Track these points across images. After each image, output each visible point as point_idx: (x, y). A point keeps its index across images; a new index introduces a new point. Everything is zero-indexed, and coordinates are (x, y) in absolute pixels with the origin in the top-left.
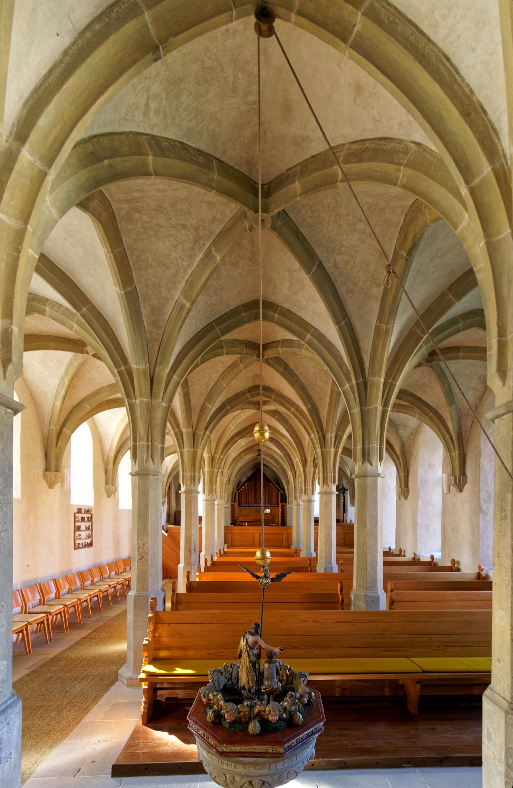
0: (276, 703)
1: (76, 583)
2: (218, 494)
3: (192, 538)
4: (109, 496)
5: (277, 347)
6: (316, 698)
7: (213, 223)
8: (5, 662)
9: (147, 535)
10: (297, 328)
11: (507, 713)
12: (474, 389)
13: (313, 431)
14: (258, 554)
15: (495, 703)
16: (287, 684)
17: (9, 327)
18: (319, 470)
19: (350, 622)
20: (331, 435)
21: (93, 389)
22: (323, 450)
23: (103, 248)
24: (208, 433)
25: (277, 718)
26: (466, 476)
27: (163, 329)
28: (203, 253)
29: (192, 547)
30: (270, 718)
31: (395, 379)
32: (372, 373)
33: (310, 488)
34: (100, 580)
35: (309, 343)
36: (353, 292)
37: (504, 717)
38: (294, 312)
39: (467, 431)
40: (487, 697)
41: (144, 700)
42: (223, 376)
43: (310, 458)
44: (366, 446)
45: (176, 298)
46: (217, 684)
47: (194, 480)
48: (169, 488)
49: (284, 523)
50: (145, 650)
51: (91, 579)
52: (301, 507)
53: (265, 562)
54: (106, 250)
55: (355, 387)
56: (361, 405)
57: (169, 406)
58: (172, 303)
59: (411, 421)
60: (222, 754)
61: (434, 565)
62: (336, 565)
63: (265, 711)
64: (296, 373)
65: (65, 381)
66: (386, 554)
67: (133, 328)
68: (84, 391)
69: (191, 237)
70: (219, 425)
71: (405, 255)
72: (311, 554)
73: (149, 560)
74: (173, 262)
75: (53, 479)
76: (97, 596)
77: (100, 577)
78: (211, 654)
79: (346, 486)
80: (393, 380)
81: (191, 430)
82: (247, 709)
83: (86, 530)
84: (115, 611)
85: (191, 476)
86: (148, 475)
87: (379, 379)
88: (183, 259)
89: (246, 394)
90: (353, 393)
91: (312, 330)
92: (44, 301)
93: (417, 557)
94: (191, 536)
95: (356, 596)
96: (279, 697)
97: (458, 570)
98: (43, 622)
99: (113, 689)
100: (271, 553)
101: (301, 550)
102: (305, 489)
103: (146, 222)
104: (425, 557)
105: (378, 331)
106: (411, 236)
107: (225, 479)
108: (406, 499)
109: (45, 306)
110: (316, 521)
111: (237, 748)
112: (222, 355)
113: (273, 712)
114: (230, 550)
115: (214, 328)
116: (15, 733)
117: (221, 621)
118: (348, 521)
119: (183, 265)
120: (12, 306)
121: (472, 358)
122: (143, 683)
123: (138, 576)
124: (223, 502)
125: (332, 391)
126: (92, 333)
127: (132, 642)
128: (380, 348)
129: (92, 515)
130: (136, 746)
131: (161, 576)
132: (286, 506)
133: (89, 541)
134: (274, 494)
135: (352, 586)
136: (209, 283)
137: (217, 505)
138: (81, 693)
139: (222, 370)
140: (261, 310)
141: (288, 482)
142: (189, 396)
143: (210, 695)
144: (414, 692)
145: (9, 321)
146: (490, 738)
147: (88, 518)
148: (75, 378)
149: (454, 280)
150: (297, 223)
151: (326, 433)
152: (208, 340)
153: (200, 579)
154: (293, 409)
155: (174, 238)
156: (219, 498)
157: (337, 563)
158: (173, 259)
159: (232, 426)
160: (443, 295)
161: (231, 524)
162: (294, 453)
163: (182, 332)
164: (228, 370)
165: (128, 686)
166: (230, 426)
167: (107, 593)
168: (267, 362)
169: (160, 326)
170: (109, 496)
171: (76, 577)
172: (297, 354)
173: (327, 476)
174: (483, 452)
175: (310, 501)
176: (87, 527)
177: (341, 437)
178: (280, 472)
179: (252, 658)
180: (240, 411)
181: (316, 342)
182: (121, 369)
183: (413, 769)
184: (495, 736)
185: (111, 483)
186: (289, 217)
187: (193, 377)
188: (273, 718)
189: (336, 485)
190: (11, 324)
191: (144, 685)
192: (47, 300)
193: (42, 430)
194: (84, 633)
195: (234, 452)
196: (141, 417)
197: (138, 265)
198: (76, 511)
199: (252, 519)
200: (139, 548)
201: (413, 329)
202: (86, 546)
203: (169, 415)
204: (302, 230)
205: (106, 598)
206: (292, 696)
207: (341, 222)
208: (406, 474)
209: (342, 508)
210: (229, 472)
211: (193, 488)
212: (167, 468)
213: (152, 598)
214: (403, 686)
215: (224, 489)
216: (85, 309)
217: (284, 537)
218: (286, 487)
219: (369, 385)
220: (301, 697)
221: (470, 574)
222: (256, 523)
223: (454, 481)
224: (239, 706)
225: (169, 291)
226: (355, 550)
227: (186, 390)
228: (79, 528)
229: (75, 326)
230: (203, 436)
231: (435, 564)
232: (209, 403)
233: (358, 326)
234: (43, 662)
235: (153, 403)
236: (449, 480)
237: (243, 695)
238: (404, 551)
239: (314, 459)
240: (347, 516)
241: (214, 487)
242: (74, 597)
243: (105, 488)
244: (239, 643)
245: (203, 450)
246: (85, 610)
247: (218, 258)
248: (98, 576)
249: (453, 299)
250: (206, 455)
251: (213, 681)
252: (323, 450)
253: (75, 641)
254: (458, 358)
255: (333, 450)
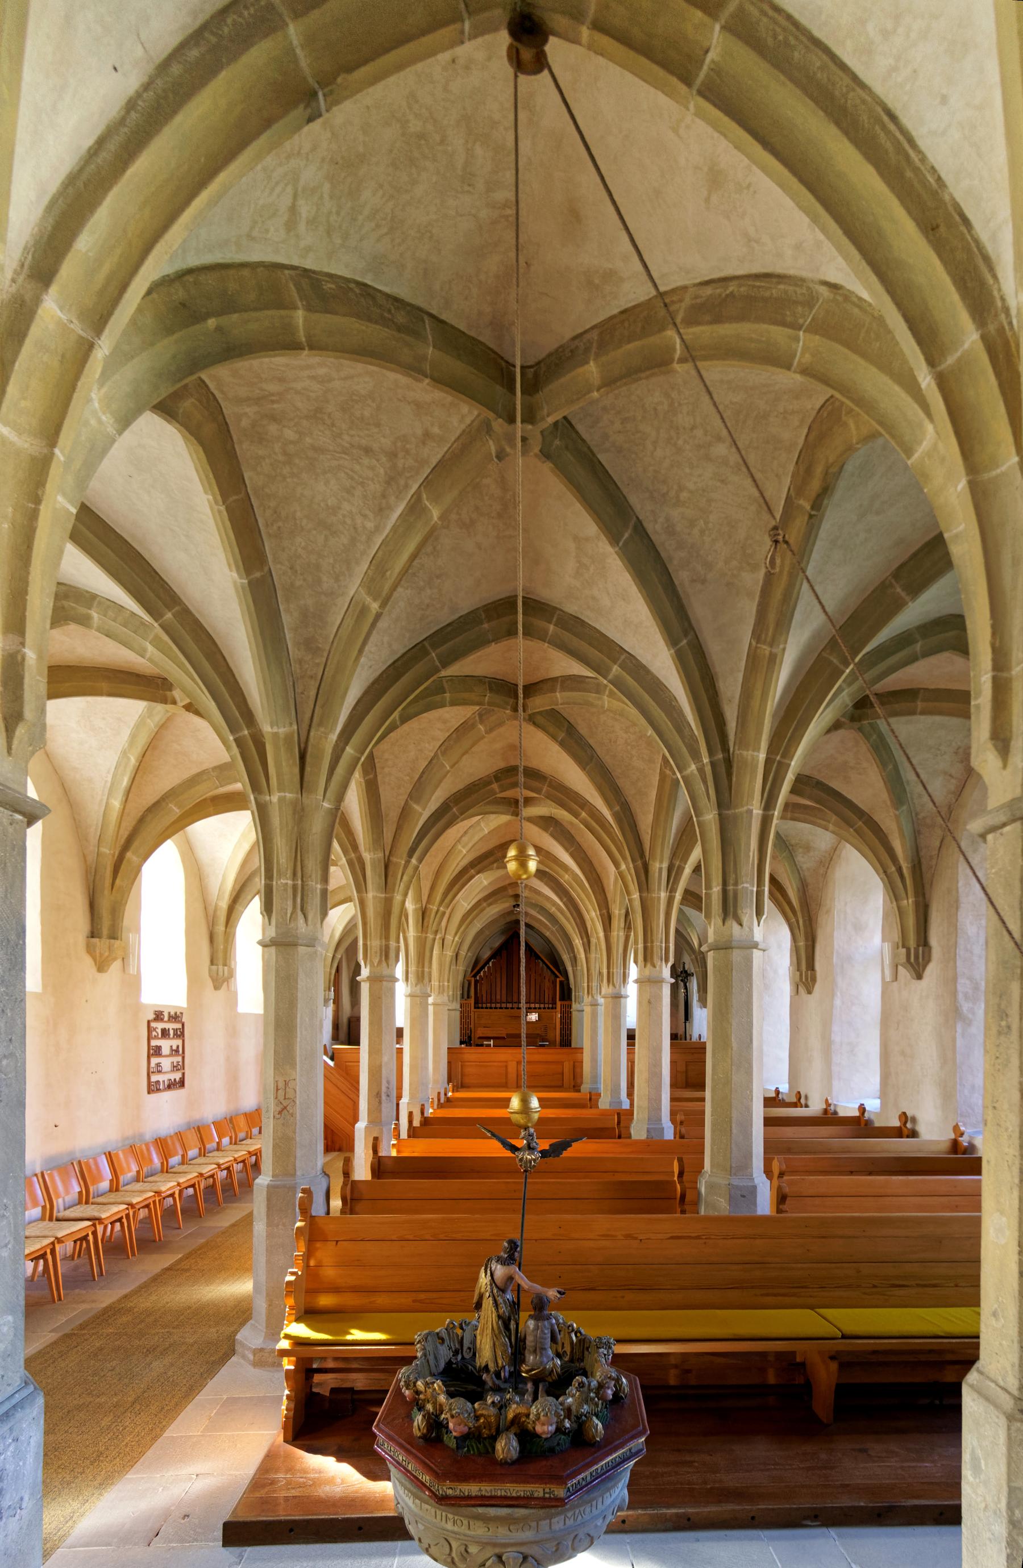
0: (551, 1399)
1: (151, 1160)
2: (435, 983)
3: (384, 1071)
4: (217, 988)
5: (553, 690)
6: (631, 1388)
7: (424, 443)
8: (10, 1318)
9: (293, 1065)
10: (593, 653)
11: (1010, 1418)
12: (945, 773)
13: (624, 858)
14: (515, 1103)
15: (987, 1399)
16: (572, 1360)
17: (18, 652)
18: (636, 936)
19: (698, 1237)
20: (659, 866)
21: (186, 775)
22: (645, 895)
23: (206, 493)
24: (414, 861)
25: (552, 1428)
26: (930, 948)
27: (325, 654)
28: (405, 502)
29: (384, 1089)
30: (539, 1429)
31: (788, 754)
32: (742, 742)
33: (617, 971)
34: (200, 1155)
35: (617, 683)
36: (704, 581)
37: (1006, 1427)
38: (586, 620)
39: (931, 857)
40: (972, 1386)
41: (287, 1392)
42: (445, 748)
43: (617, 912)
44: (730, 888)
45: (352, 593)
46: (432, 1362)
47: (387, 955)
48: (338, 970)
49: (566, 1041)
50: (289, 1293)
51: (180, 1152)
52: (601, 1010)
53: (529, 1119)
54: (211, 497)
55: (708, 769)
56: (720, 805)
57: (337, 809)
58: (343, 603)
59: (819, 837)
60: (442, 1500)
61: (866, 1125)
62: (670, 1124)
63: (528, 1416)
64: (591, 742)
65: (129, 759)
66: (770, 1102)
67: (266, 654)
68: (167, 777)
69: (382, 471)
70: (436, 845)
71: (808, 508)
72: (620, 1103)
73: (298, 1115)
74: (345, 522)
75: (107, 954)
76: (193, 1186)
77: (200, 1149)
78: (420, 1301)
79: (690, 967)
80: (783, 756)
81: (380, 855)
82: (493, 1411)
83: (171, 1055)
84: (230, 1216)
85: (381, 946)
86: (295, 945)
87: (756, 754)
88: (365, 516)
89: (490, 783)
90: (705, 782)
91: (623, 657)
92: (89, 598)
93: (832, 1107)
94: (380, 1066)
95: (711, 1186)
96: (557, 1386)
97: (914, 1134)
98: (85, 1238)
99: (224, 1371)
100: (540, 1100)
101: (600, 1095)
102: (608, 973)
103: (291, 442)
104: (848, 1108)
105: (753, 658)
106: (819, 470)
107: (449, 953)
108: (810, 992)
109: (90, 609)
110: (631, 1036)
111: (473, 1489)
112: (443, 706)
113: (543, 1416)
114: (458, 1095)
115: (427, 653)
116: (30, 1459)
117: (442, 1237)
118: (695, 1037)
119: (364, 527)
120: (25, 609)
121: (941, 713)
122: (285, 1360)
123: (276, 1146)
124: (445, 998)
125: (663, 777)
126: (183, 663)
127: (263, 1278)
128: (758, 693)
129: (183, 1025)
130: (271, 1484)
131: (321, 1147)
132: (570, 1006)
133: (177, 1076)
134: (547, 984)
135: (702, 1166)
136: (416, 563)
137: (433, 1004)
138: (162, 1380)
139: (443, 736)
140: (520, 617)
141: (574, 960)
142: (377, 788)
143: (419, 1383)
144: (826, 1377)
145: (17, 639)
146: (976, 1469)
147: (175, 1030)
148: (150, 752)
149: (905, 557)
150: (592, 444)
151: (651, 862)
152: (415, 677)
153: (398, 1152)
154: (584, 814)
155: (347, 474)
156: (437, 990)
157: (673, 1120)
158: (344, 516)
159: (463, 847)
160: (883, 587)
161: (461, 1043)
162: (587, 902)
163: (363, 660)
164: (454, 735)
165: (255, 1364)
166: (460, 847)
167: (214, 1180)
168: (532, 719)
169: (318, 648)
170: (217, 988)
171: (152, 1149)
172: (592, 705)
173: (652, 947)
174: (963, 899)
175: (618, 998)
176: (174, 1048)
177: (680, 870)
178: (558, 940)
179: (503, 1309)
180: (479, 817)
181: (630, 681)
182: (241, 734)
183: (824, 1530)
184: (986, 1464)
185: (221, 961)
186: (577, 432)
187: (385, 751)
188: (545, 1429)
189: (670, 964)
190: (23, 644)
191: (288, 1364)
192: (93, 597)
193: (84, 856)
194: (167, 1260)
195: (466, 899)
196: (281, 830)
197: (275, 527)
198: (152, 1016)
199: (503, 1033)
200: (277, 1090)
201: (824, 654)
202: (171, 1086)
203: (337, 825)
204: (602, 457)
205: (211, 1189)
206: (581, 1385)
207: (680, 442)
208: (810, 943)
209: (682, 1011)
210: (456, 939)
211: (386, 972)
212: (333, 930)
213: (304, 1191)
214: (803, 1365)
215: (447, 972)
216: (169, 615)
217: (567, 1068)
218: (570, 969)
219: (735, 766)
220: (601, 1386)
221: (938, 1142)
222: (510, 1040)
223: (905, 956)
224: (476, 1405)
225: (337, 579)
226: (708, 1094)
227: (371, 776)
228: (157, 1051)
229: (150, 648)
230: (406, 867)
231: (868, 1123)
232: (418, 801)
233: (714, 648)
234: (86, 1318)
235: (306, 801)
236: (894, 956)
237: (484, 1383)
238: (806, 1097)
239: (627, 914)
240: (692, 1026)
241: (426, 970)
242: (148, 1188)
243: (210, 970)
244: (476, 1279)
245: (406, 895)
246: (170, 1213)
247: (435, 514)
248: (195, 1147)
249: (903, 594)
250: (410, 906)
251: (425, 1355)
252: (645, 895)
253: (150, 1275)
254: (912, 713)
255: (663, 895)
